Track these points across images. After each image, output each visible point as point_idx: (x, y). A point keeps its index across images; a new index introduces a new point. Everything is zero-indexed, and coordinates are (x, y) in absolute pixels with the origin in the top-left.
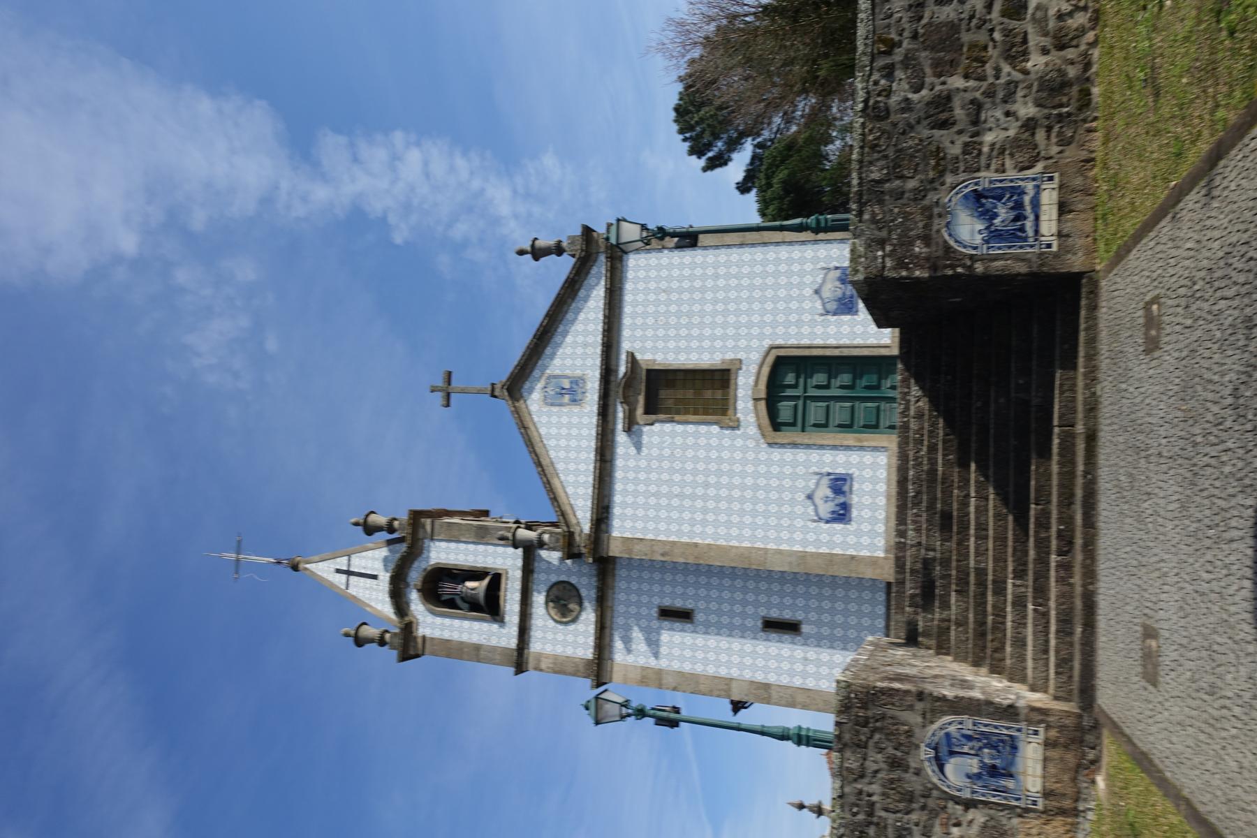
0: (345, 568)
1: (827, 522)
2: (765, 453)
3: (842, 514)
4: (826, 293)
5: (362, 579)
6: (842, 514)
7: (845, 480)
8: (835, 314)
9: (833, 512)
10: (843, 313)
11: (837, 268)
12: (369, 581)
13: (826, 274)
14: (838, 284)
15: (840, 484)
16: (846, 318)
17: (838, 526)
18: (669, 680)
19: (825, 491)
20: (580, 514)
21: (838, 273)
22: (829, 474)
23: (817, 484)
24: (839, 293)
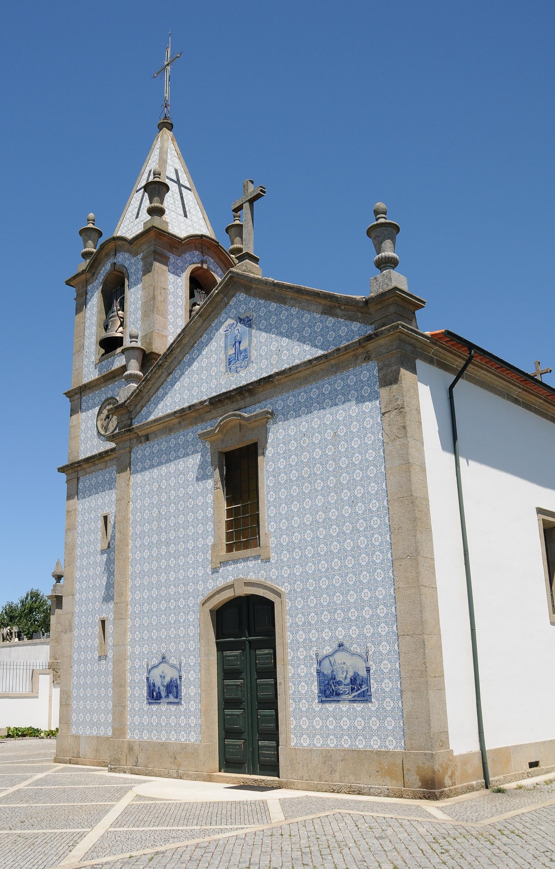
0: (464, 362)
1: (148, 679)
2: (195, 602)
3: (329, 690)
4: (340, 657)
5: (180, 205)
6: (329, 690)
7: (177, 697)
8: (319, 672)
9: (154, 685)
10: (320, 683)
11: (368, 670)
12: (182, 212)
13: (360, 656)
14: (351, 674)
15: (359, 688)
16: (315, 688)
17: (145, 692)
18: (231, 562)
19: (170, 674)
20: (168, 400)
21: (363, 673)
22: (180, 677)
23: (173, 666)
24: (340, 677)
